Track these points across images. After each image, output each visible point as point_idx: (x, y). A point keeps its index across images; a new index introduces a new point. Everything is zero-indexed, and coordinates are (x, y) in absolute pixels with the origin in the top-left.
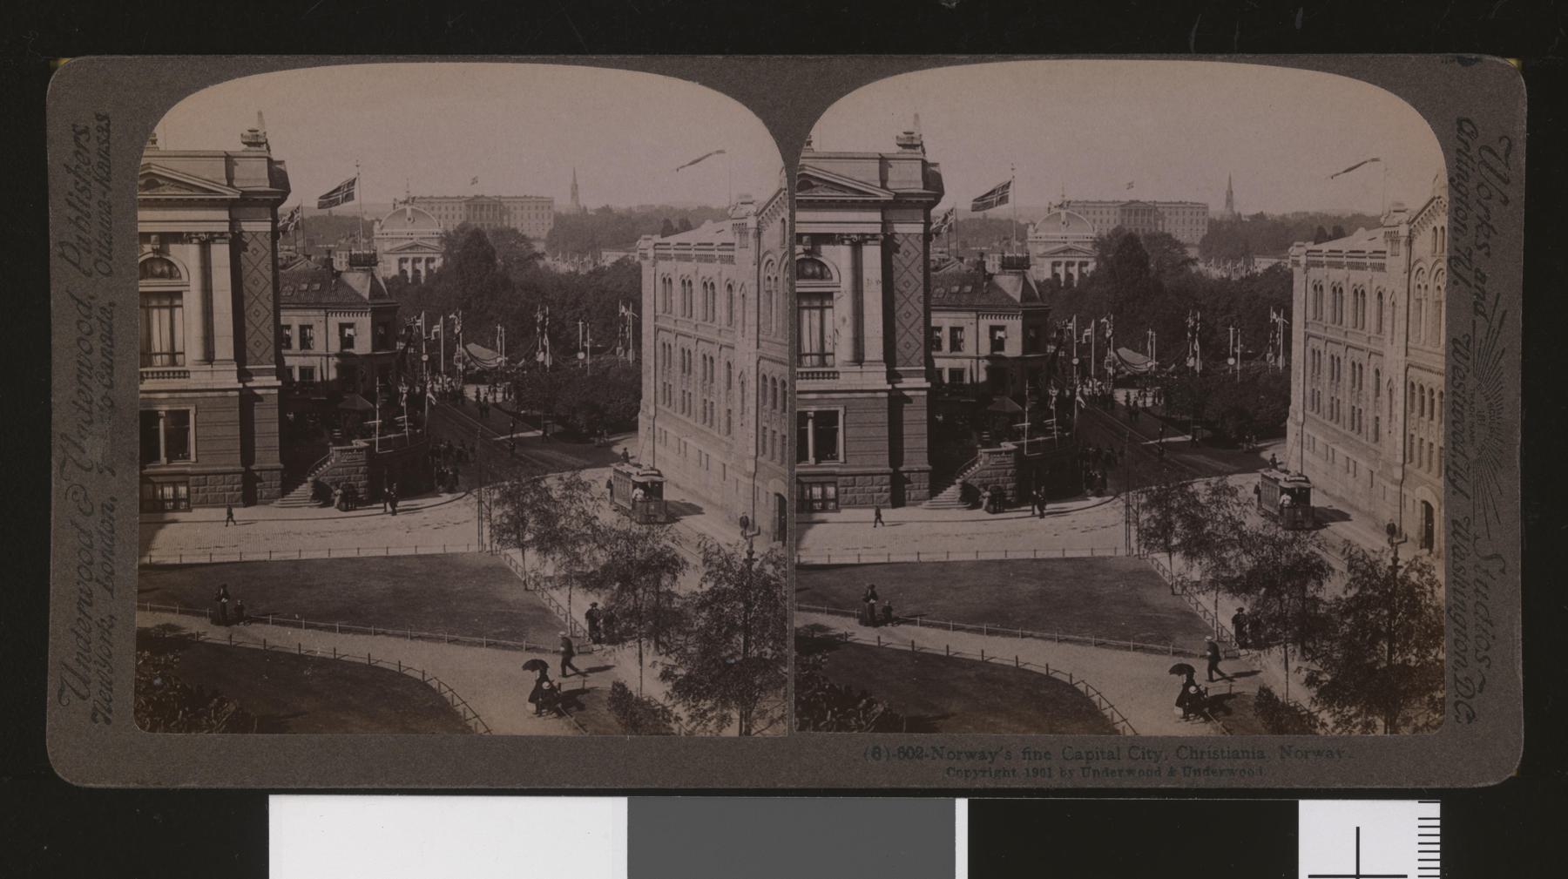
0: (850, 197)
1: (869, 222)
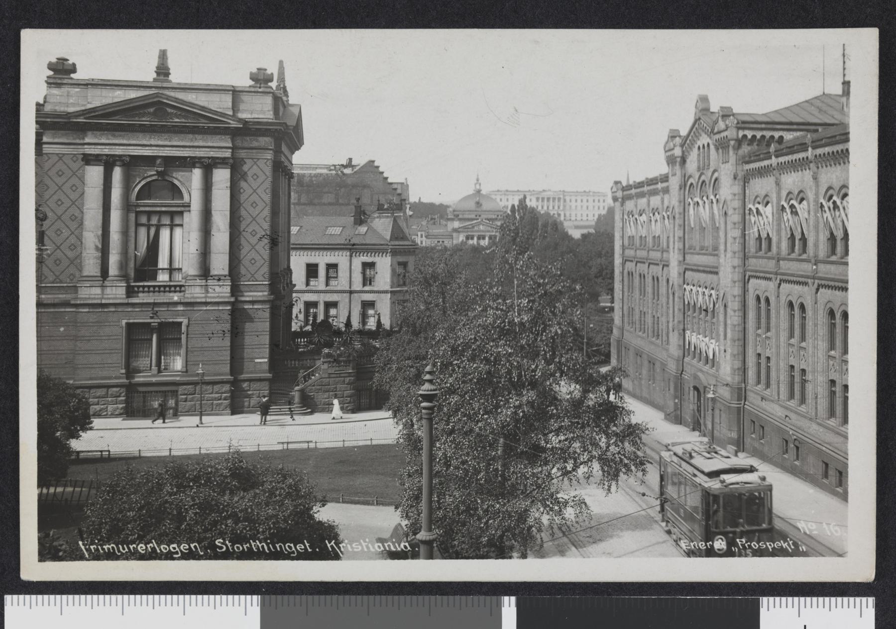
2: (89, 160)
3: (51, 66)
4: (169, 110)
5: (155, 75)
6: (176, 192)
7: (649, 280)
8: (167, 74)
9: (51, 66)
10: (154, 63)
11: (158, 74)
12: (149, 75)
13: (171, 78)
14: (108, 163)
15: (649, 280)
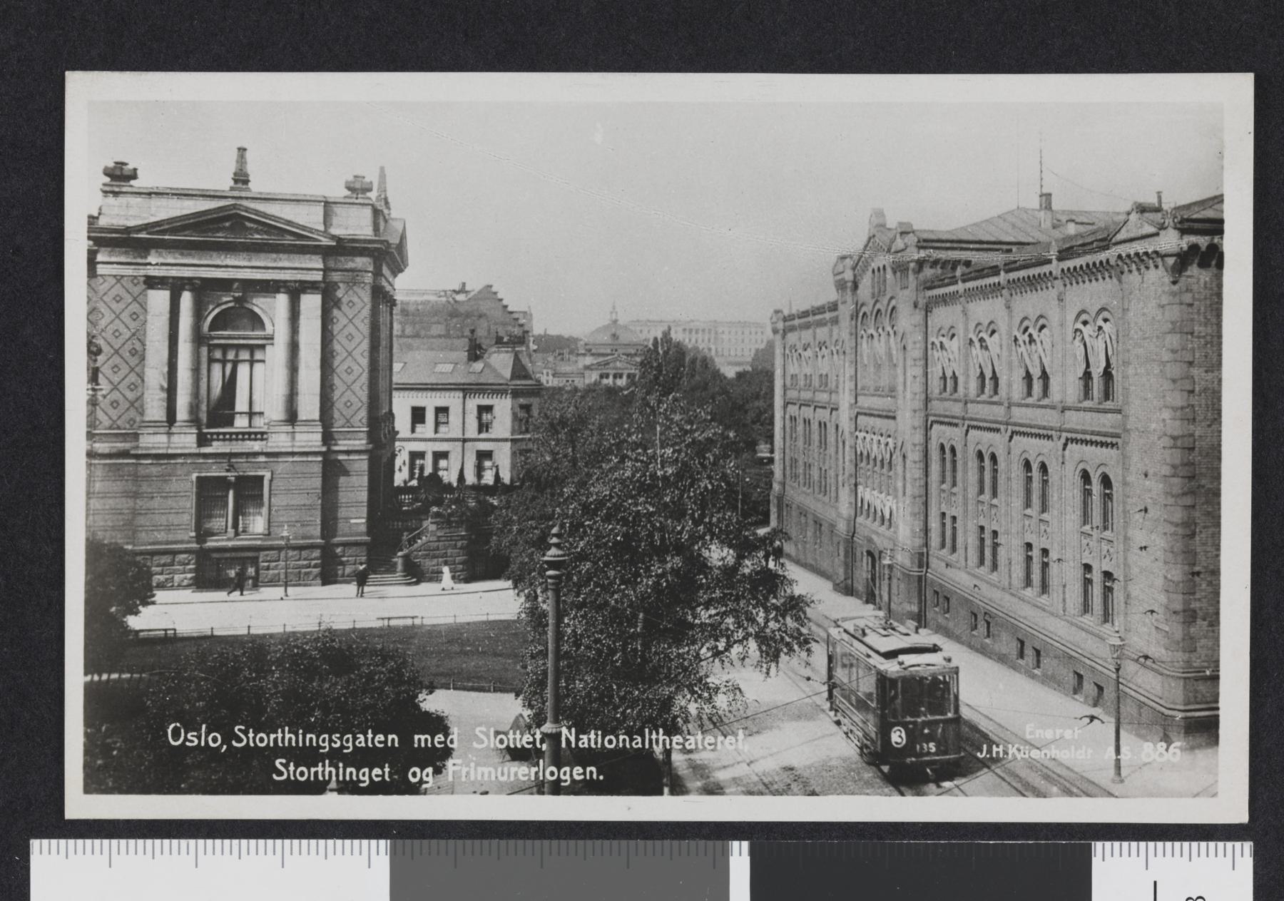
2: (152, 283)
3: (108, 172)
4: (248, 224)
5: (232, 183)
8: (246, 182)
9: (108, 172)
10: (232, 168)
11: (236, 181)
12: (224, 183)
13: (250, 185)
14: (176, 287)
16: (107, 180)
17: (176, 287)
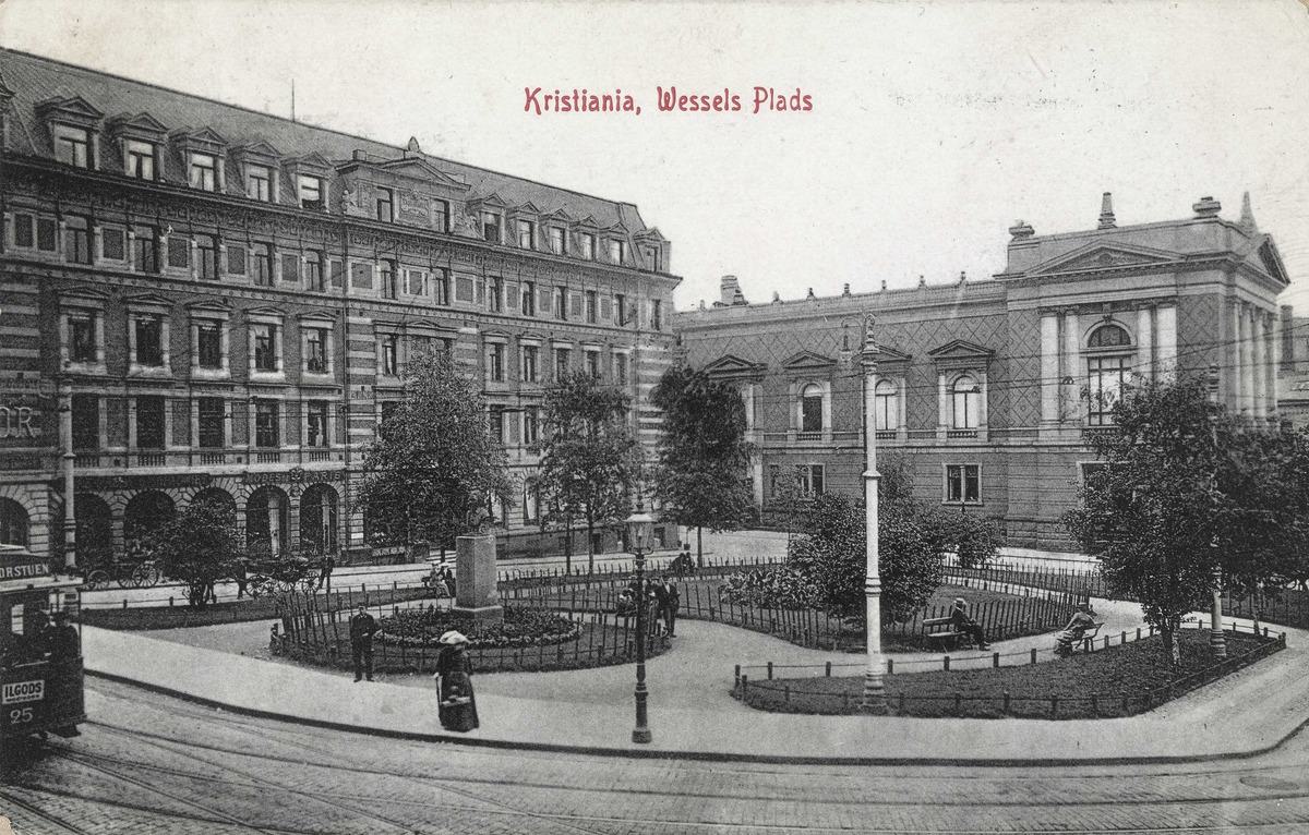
0: (1143, 263)
1: (1157, 285)
2: (1044, 311)
4: (1113, 255)
6: (1124, 338)
7: (528, 312)
15: (528, 312)
16: (1011, 237)
17: (1061, 314)
